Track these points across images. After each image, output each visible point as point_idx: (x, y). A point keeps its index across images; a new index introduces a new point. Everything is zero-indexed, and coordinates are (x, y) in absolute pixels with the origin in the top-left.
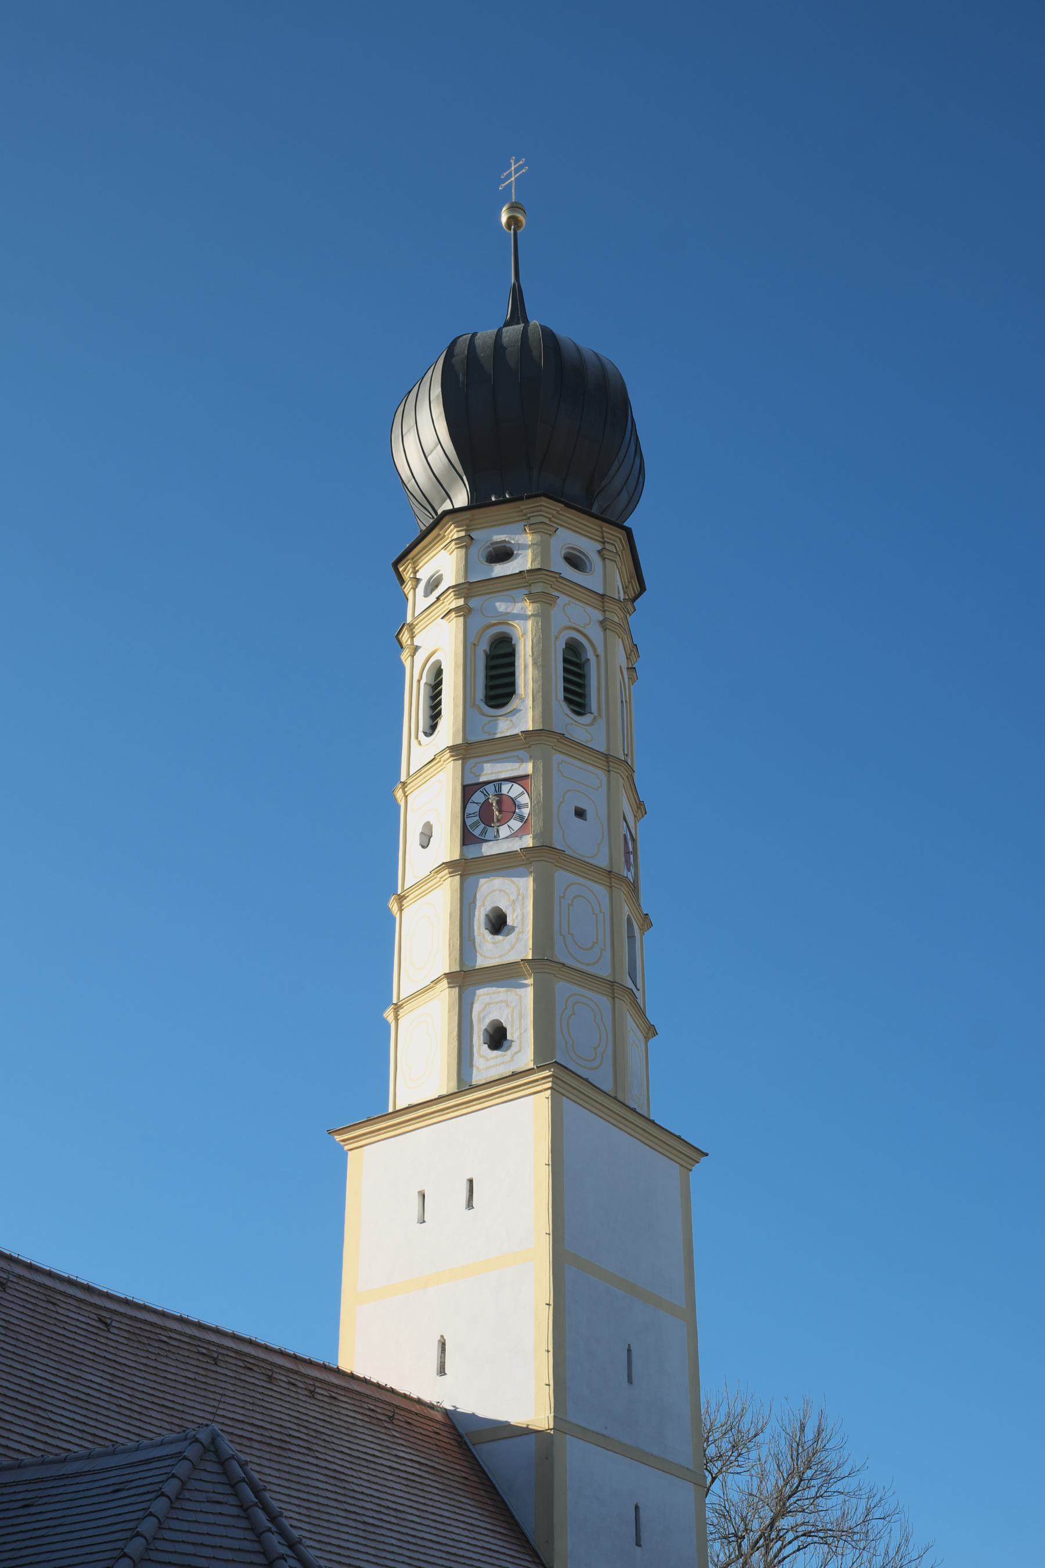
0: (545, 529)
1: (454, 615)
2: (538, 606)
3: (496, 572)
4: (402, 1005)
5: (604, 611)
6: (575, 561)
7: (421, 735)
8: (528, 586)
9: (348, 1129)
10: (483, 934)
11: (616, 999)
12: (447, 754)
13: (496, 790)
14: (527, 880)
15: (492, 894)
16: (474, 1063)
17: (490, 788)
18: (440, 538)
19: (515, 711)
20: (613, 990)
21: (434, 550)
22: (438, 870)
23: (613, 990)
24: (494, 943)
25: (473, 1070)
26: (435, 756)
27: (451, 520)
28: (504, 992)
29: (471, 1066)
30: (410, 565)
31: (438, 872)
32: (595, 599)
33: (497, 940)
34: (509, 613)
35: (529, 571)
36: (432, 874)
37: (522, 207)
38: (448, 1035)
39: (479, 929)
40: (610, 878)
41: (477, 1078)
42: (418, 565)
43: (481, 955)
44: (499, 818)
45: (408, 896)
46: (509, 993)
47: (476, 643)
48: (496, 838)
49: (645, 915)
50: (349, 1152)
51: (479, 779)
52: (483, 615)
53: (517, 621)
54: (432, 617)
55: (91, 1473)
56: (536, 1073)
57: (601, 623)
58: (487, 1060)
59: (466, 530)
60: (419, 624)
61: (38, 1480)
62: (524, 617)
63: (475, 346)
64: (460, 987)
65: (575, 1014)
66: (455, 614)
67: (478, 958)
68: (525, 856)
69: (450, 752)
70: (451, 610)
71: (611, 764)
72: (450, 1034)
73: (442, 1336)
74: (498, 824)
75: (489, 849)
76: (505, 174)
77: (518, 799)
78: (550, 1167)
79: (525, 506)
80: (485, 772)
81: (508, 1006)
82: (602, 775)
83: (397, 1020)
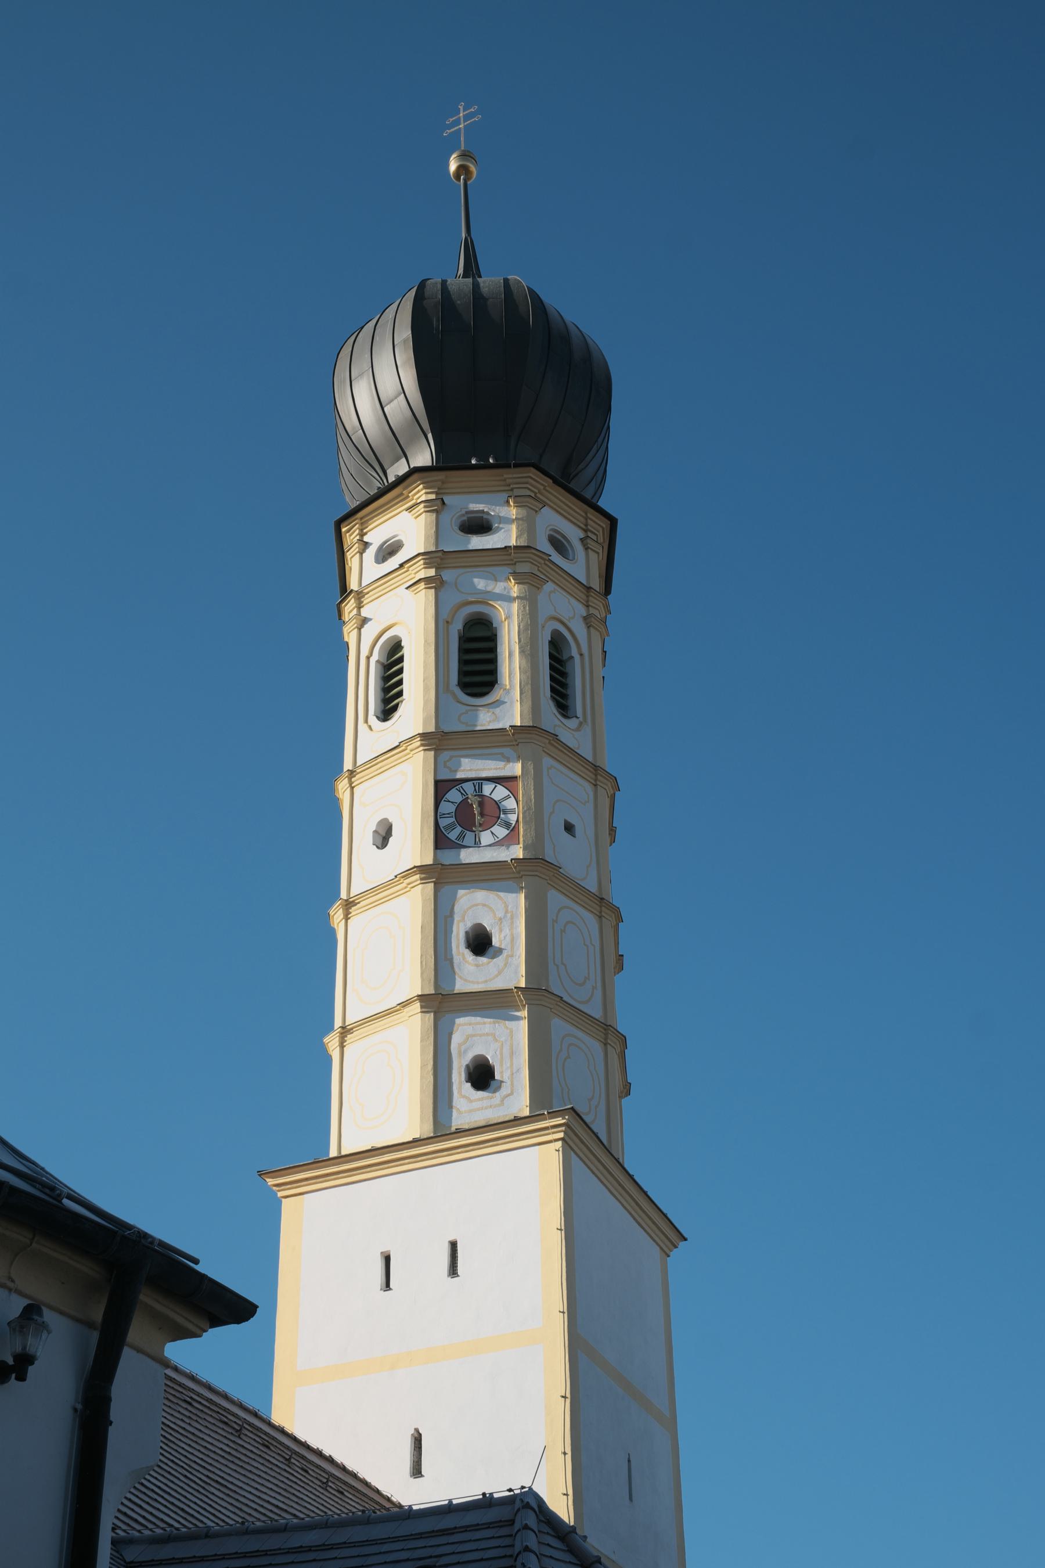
0: (532, 504)
1: (424, 586)
2: (524, 588)
3: (472, 545)
4: (352, 1029)
5: (588, 606)
6: (558, 543)
7: (373, 720)
8: (512, 564)
9: (290, 1171)
10: (463, 954)
11: (608, 1046)
12: (417, 743)
13: (475, 789)
14: (517, 897)
15: (475, 908)
16: (454, 1104)
17: (468, 787)
18: (402, 498)
19: (498, 703)
20: (606, 1034)
21: (390, 513)
22: (407, 874)
23: (606, 1034)
24: (477, 966)
25: (452, 1112)
26: (400, 743)
27: (420, 480)
28: (490, 1023)
29: (451, 1107)
30: (357, 526)
31: (405, 877)
32: (579, 590)
33: (481, 963)
34: (489, 592)
35: (516, 547)
36: (397, 879)
37: (473, 157)
38: (421, 1067)
39: (458, 947)
40: (601, 907)
41: (458, 1121)
42: (367, 527)
43: (461, 978)
44: (481, 822)
45: (359, 903)
46: (497, 1025)
47: (450, 620)
48: (477, 844)
49: (620, 955)
50: (283, 1200)
51: (456, 775)
52: (458, 590)
53: (499, 602)
54: (392, 585)
55: (347, 1545)
56: (547, 1120)
57: (585, 618)
58: (471, 1101)
59: (437, 493)
60: (371, 593)
61: (344, 1546)
62: (510, 599)
63: (449, 292)
64: (435, 1013)
65: (570, 1058)
66: (425, 584)
67: (456, 981)
68: (515, 868)
69: (421, 740)
70: (420, 580)
71: (599, 777)
72: (423, 1066)
73: (417, 1430)
74: (480, 829)
75: (468, 856)
76: (451, 120)
77: (502, 803)
78: (563, 1232)
79: (509, 474)
80: (462, 768)
81: (496, 1040)
82: (589, 788)
83: (342, 1046)
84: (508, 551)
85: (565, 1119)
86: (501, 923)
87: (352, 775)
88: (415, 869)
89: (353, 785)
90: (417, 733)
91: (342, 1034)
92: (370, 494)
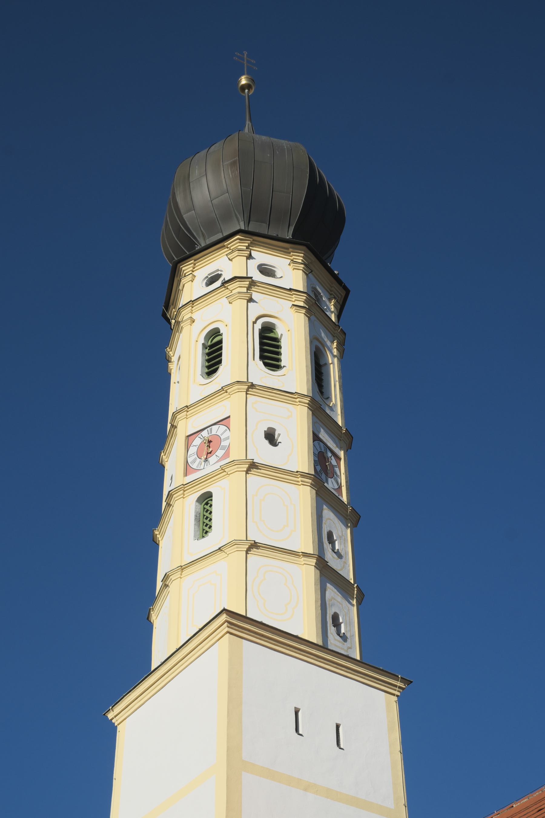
4: (260, 546)
26: (296, 393)
27: (304, 251)
30: (250, 242)
42: (253, 247)
45: (260, 469)
60: (260, 288)
84: (336, 327)
85: (406, 686)
86: (340, 539)
87: (251, 387)
88: (313, 476)
89: (248, 392)
90: (236, 381)
91: (251, 545)
92: (248, 229)
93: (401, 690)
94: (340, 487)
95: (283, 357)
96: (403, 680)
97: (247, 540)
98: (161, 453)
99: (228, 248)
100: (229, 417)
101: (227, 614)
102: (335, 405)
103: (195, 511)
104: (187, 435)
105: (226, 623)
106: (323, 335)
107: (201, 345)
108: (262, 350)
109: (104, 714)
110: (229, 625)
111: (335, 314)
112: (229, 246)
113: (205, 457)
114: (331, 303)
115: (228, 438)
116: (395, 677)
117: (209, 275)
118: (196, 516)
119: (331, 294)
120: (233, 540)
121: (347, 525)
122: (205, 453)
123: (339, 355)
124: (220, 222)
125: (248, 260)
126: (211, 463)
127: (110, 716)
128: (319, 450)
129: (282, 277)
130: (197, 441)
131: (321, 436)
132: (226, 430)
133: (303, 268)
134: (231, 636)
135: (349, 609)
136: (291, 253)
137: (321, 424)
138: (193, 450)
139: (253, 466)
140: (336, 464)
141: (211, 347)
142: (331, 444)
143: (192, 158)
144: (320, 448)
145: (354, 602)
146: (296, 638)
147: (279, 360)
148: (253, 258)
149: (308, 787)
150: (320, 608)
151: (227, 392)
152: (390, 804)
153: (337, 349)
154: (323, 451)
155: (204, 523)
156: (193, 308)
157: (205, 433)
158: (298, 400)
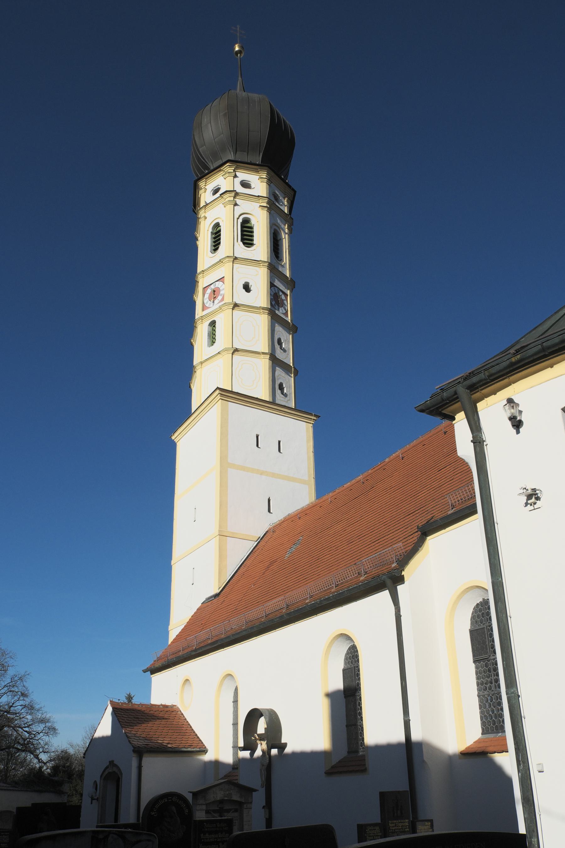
1: (266, 210)
4: (239, 350)
26: (260, 260)
30: (235, 167)
42: (237, 170)
45: (240, 307)
60: (241, 196)
69: (268, 264)
93: (314, 421)
94: (287, 312)
95: (255, 238)
96: (315, 416)
97: (232, 348)
98: (193, 295)
99: (223, 171)
100: (224, 277)
101: (219, 390)
102: (285, 264)
103: (208, 331)
104: (204, 287)
105: (219, 394)
106: (279, 221)
107: (210, 233)
108: (242, 235)
109: (170, 437)
110: (221, 395)
111: (287, 207)
112: (223, 170)
113: (213, 300)
114: (285, 200)
115: (223, 289)
116: (311, 414)
117: (214, 188)
118: (208, 334)
119: (285, 194)
120: (225, 348)
121: (290, 333)
122: (213, 298)
123: (289, 232)
124: (220, 152)
125: (235, 179)
126: (215, 304)
127: (173, 438)
128: (274, 292)
129: (254, 188)
130: (209, 291)
131: (275, 284)
132: (223, 285)
133: (267, 181)
134: (222, 400)
135: (289, 380)
136: (260, 172)
137: (275, 276)
138: (207, 296)
139: (236, 305)
140: (285, 299)
141: (216, 233)
142: (282, 287)
143: (203, 111)
144: (275, 291)
145: (293, 375)
146: (257, 399)
147: (252, 240)
148: (237, 177)
149: (262, 473)
150: (271, 381)
151: (222, 262)
152: (306, 478)
153: (288, 229)
154: (277, 292)
155: (213, 337)
156: (205, 209)
157: (212, 286)
158: (261, 264)
